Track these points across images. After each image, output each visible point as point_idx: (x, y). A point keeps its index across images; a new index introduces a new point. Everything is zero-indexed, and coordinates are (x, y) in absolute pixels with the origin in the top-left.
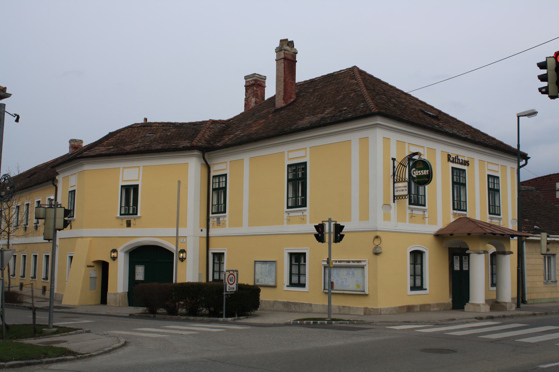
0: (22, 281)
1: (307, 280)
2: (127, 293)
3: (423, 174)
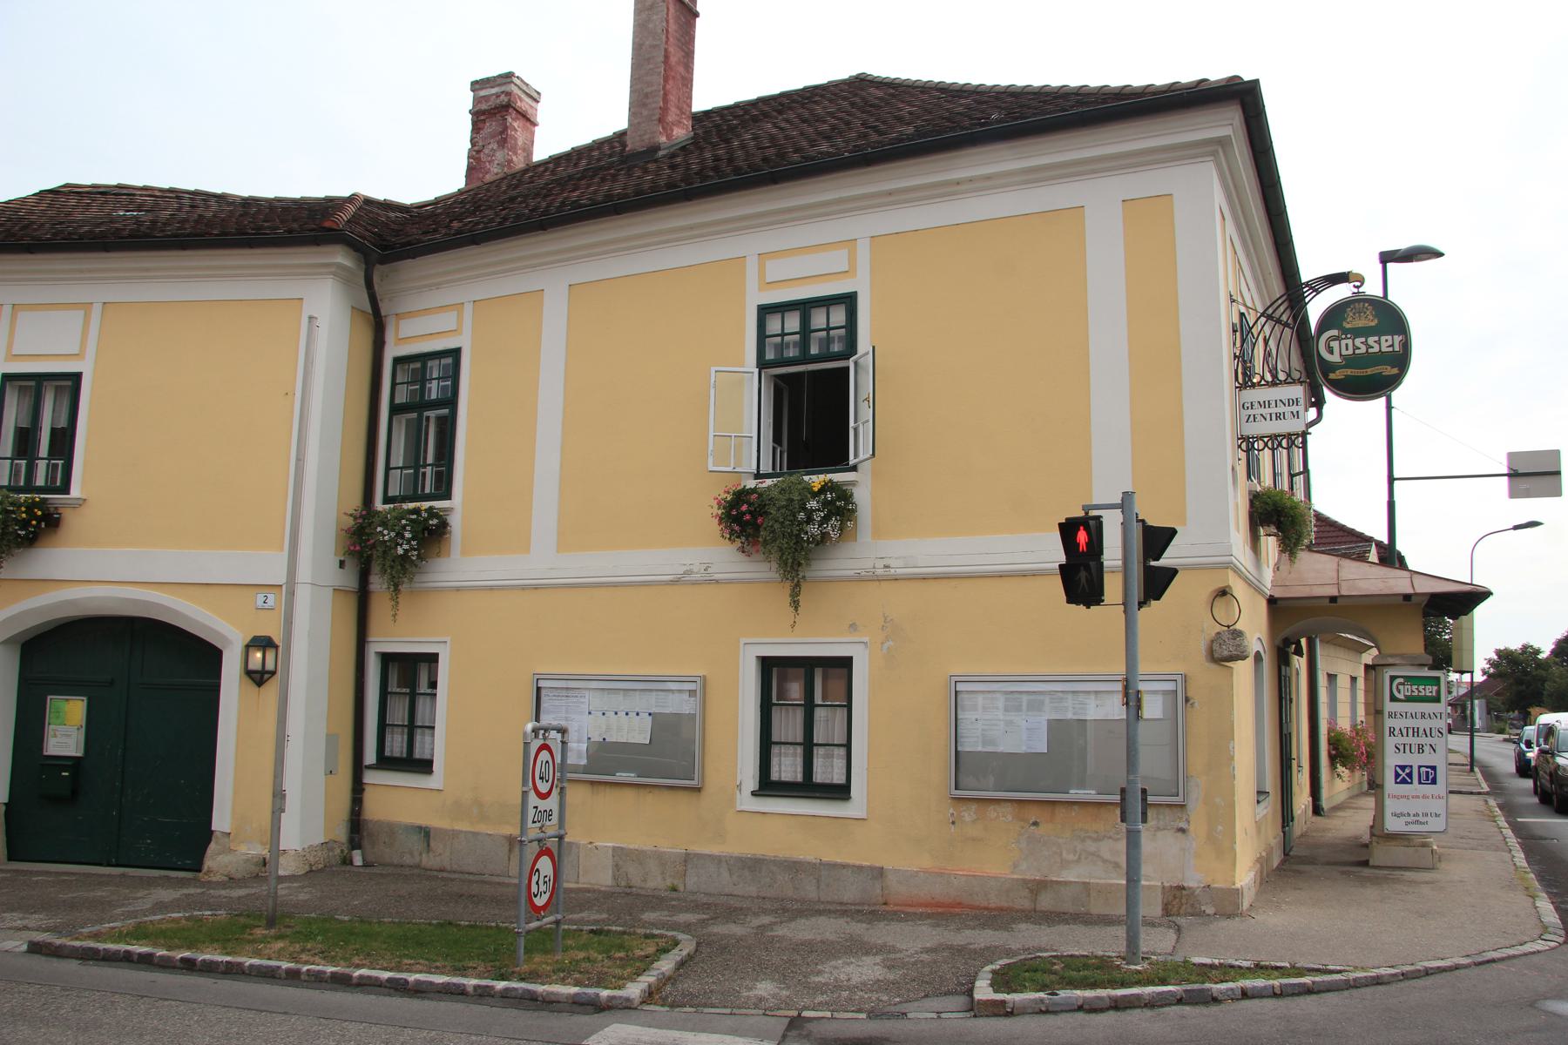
2: (4, 808)
3: (1376, 349)
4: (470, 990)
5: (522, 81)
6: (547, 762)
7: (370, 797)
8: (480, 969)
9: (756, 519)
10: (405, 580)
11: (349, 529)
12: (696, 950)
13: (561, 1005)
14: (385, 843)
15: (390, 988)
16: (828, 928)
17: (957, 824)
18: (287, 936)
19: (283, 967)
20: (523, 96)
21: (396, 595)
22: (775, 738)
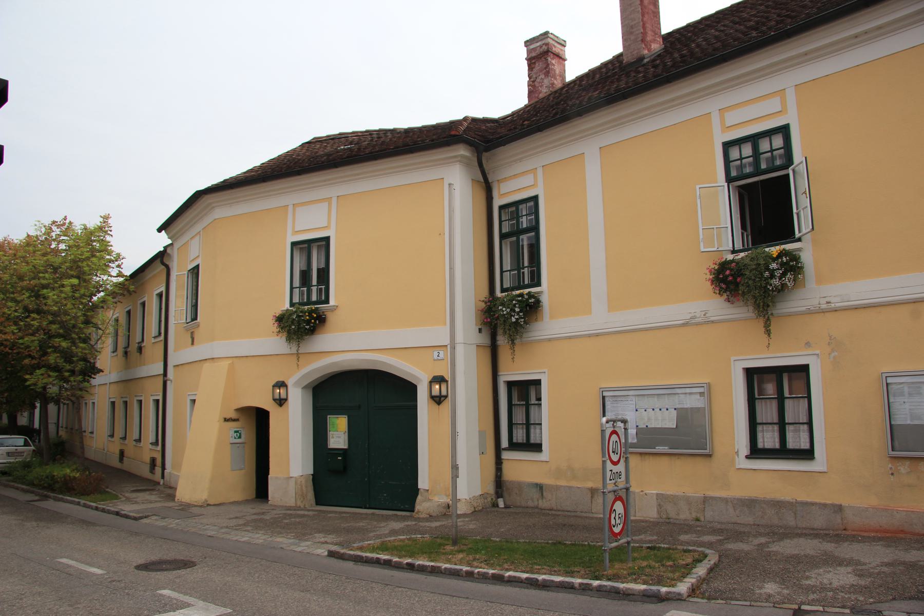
0: (123, 447)
2: (311, 477)
4: (577, 586)
5: (554, 35)
6: (616, 441)
7: (506, 467)
8: (582, 572)
9: (736, 279)
10: (518, 337)
11: (483, 309)
12: (719, 561)
13: (636, 596)
14: (516, 494)
15: (527, 584)
16: (809, 547)
17: (895, 474)
18: (465, 551)
19: (464, 570)
20: (556, 44)
21: (513, 346)
22: (759, 420)
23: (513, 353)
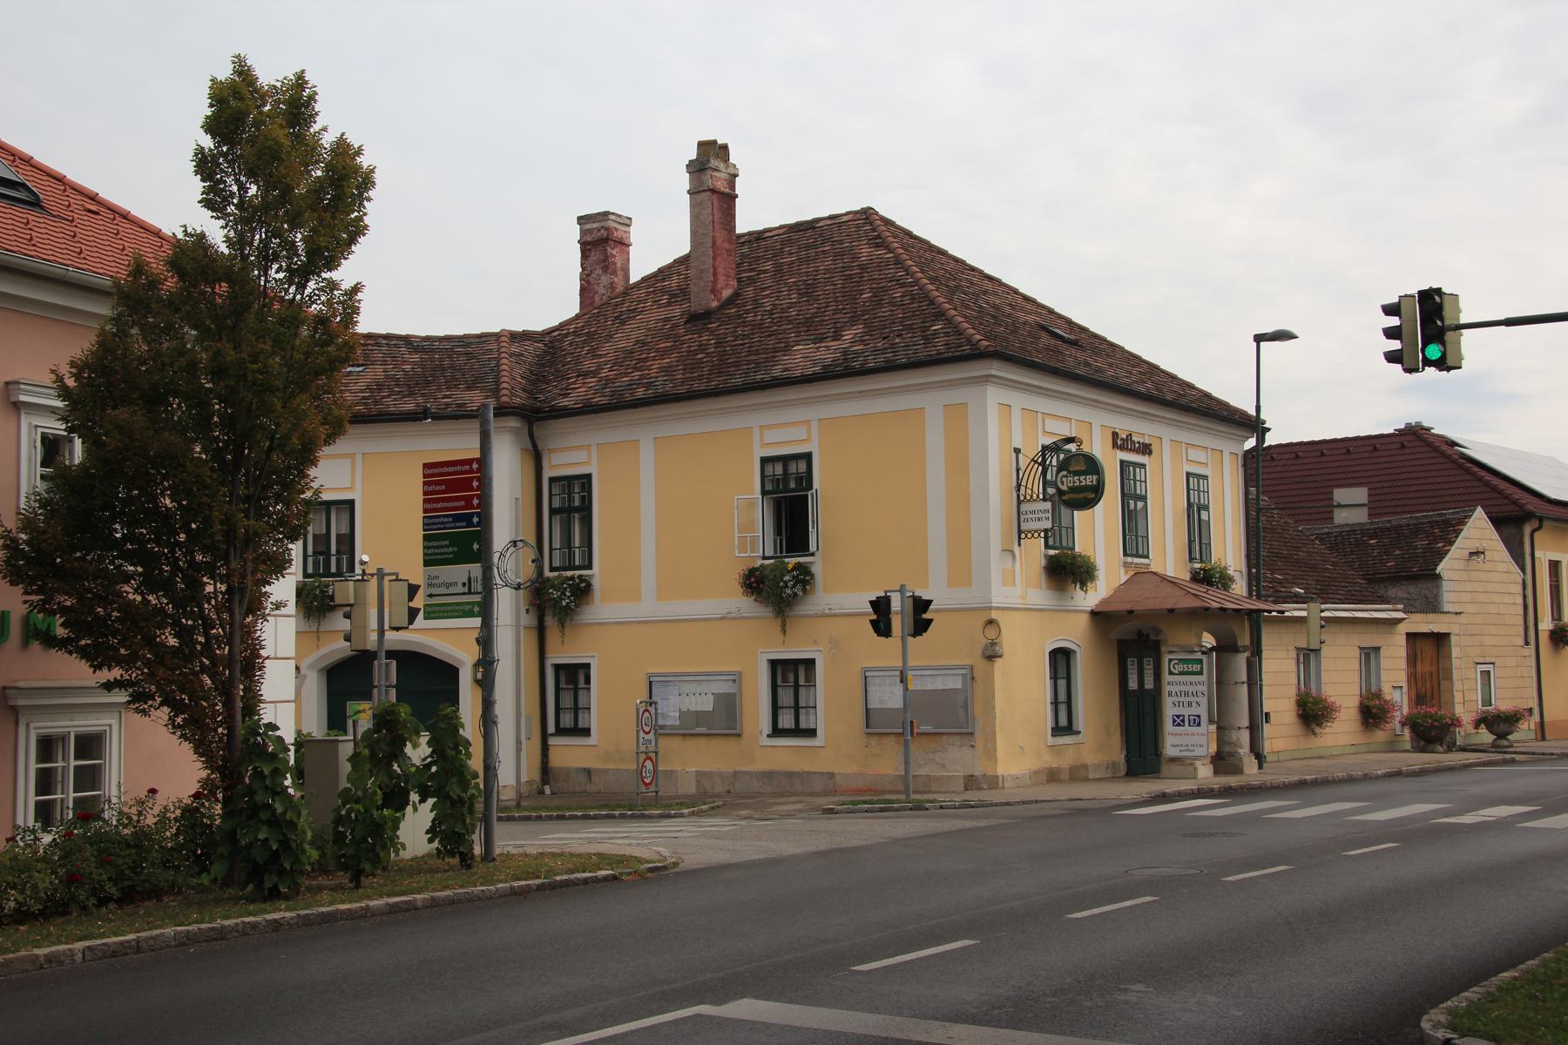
1: (820, 719)
3: (1084, 484)
20: (618, 226)
22: (780, 704)
23: (562, 632)
